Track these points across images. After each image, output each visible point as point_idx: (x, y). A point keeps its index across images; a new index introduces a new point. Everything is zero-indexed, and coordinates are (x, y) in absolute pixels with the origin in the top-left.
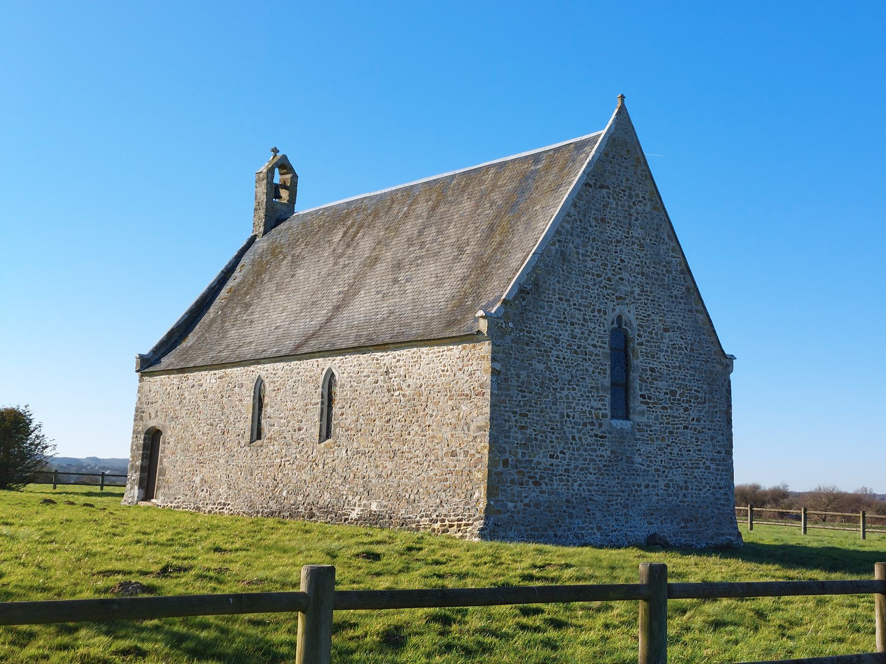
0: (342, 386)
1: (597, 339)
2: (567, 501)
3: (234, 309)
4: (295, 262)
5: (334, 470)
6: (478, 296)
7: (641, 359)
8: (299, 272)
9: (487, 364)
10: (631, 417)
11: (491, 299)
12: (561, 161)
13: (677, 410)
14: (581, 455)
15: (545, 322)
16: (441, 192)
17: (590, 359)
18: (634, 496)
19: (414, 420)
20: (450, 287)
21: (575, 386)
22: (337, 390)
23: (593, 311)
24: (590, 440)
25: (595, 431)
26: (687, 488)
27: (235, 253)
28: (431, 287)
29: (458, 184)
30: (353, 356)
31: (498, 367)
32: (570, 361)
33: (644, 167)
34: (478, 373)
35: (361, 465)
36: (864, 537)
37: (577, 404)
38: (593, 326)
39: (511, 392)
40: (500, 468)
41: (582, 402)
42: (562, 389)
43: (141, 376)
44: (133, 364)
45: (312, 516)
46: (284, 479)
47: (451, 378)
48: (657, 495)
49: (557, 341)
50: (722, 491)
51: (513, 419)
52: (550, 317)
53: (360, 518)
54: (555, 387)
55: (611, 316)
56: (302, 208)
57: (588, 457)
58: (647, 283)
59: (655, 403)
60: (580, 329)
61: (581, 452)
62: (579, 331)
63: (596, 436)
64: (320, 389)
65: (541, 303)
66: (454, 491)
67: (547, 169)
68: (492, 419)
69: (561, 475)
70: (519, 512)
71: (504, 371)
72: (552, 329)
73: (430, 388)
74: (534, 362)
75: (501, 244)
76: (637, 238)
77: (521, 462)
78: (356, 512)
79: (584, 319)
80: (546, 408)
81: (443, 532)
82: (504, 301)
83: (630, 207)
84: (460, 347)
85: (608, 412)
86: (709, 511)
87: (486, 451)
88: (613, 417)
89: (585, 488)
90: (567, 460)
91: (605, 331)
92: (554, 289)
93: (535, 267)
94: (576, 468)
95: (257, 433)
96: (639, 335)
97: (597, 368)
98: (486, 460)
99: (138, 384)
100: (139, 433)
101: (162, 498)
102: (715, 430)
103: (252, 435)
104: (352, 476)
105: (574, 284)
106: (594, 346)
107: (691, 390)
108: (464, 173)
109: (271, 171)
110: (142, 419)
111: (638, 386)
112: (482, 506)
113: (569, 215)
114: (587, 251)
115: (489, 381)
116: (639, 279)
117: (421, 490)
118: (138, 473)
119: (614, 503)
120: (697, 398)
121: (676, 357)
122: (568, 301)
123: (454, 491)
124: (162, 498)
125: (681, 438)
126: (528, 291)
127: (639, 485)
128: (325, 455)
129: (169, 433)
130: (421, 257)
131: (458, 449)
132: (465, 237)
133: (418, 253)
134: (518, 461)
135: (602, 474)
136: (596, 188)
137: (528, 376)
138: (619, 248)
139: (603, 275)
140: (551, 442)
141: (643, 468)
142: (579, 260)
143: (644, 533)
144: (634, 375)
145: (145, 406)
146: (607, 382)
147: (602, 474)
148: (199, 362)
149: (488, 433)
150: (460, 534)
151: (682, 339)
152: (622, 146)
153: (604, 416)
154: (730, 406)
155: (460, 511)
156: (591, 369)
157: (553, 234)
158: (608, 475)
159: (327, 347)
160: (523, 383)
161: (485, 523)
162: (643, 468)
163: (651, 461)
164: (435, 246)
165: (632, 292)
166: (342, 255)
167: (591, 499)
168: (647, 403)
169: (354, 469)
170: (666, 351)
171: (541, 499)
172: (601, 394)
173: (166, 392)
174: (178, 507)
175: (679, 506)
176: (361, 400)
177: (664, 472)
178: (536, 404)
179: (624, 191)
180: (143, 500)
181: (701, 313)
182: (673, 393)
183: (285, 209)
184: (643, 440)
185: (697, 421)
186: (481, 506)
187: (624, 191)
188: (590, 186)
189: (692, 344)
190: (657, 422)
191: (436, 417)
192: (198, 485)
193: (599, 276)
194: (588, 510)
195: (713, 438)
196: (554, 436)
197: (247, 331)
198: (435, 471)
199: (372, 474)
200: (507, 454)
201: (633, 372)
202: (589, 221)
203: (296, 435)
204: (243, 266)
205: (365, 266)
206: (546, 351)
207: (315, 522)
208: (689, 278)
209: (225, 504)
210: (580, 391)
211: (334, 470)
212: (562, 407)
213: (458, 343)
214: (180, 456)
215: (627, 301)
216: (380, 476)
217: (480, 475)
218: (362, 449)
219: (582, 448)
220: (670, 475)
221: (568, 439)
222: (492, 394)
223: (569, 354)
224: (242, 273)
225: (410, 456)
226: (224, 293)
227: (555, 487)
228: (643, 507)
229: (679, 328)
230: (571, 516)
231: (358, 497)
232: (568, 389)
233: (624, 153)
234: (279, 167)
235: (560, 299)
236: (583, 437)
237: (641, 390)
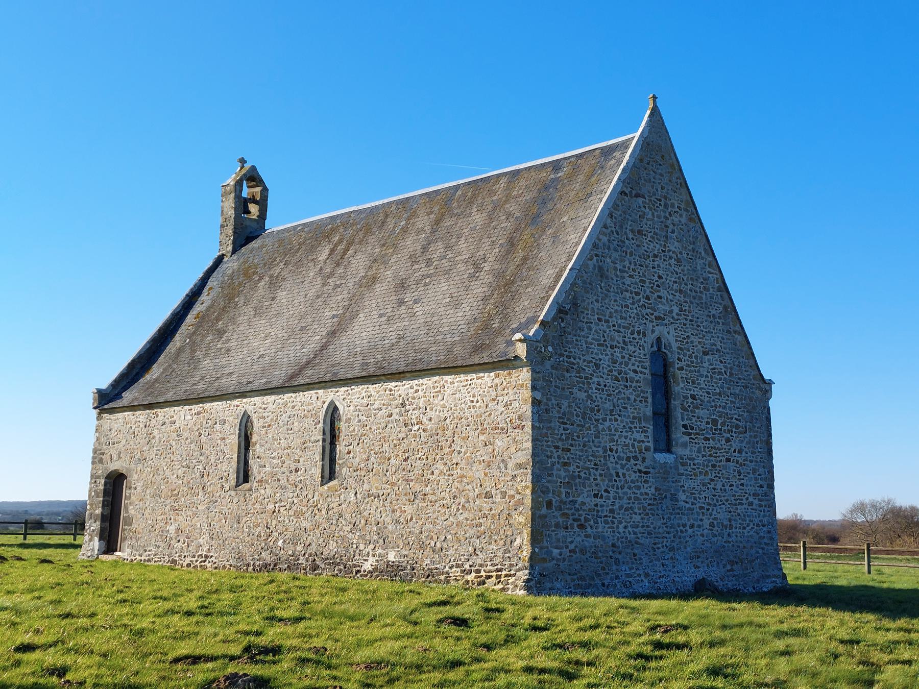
0: (348, 421)
1: (637, 364)
2: (613, 545)
3: (205, 336)
4: (275, 283)
5: (341, 516)
6: (505, 318)
7: (682, 385)
8: (280, 294)
9: (527, 394)
10: (673, 449)
11: (523, 320)
12: (587, 169)
13: (719, 441)
14: (625, 493)
15: (584, 346)
16: (445, 204)
17: (631, 386)
18: (680, 538)
19: (437, 458)
20: (469, 307)
21: (617, 416)
22: (342, 425)
23: (632, 333)
24: (634, 476)
25: (638, 467)
26: (731, 527)
27: (201, 275)
28: (447, 307)
29: (464, 195)
30: (361, 387)
31: (539, 396)
32: (611, 389)
33: (679, 174)
34: (515, 404)
35: (373, 509)
36: (869, 572)
37: (620, 436)
38: (633, 349)
39: (552, 425)
40: (544, 511)
41: (624, 434)
42: (604, 420)
43: (100, 414)
44: (89, 400)
45: (315, 568)
46: (280, 527)
47: (482, 410)
48: (702, 535)
49: (597, 366)
50: (765, 529)
51: (556, 455)
52: (589, 340)
53: (375, 570)
54: (596, 417)
55: (651, 338)
56: (273, 225)
57: (633, 496)
58: (686, 302)
59: (697, 434)
60: (620, 352)
61: (626, 490)
62: (620, 355)
63: (640, 471)
64: (321, 425)
65: (580, 324)
66: (490, 537)
67: (570, 177)
68: (534, 455)
69: (606, 516)
70: (564, 560)
71: (545, 401)
72: (592, 353)
73: (456, 421)
74: (575, 390)
75: (525, 259)
76: (674, 252)
77: (565, 503)
78: (370, 563)
79: (624, 342)
80: (589, 441)
81: (479, 584)
82: (543, 323)
83: (667, 218)
84: (492, 374)
85: (651, 444)
86: (753, 551)
87: (528, 492)
88: (656, 450)
89: (630, 529)
90: (612, 500)
91: (645, 355)
92: (593, 308)
93: (574, 284)
94: (621, 507)
95: (244, 475)
96: (679, 359)
97: (638, 396)
98: (528, 501)
99: (96, 422)
100: (98, 477)
101: (128, 551)
102: (756, 462)
103: (238, 478)
104: (363, 522)
105: (612, 302)
106: (635, 371)
107: (732, 418)
108: (469, 183)
109: (239, 184)
110: (101, 461)
111: (679, 415)
112: (526, 553)
113: (605, 227)
114: (624, 267)
115: (529, 413)
116: (677, 297)
117: (449, 537)
118: (98, 523)
119: (660, 546)
120: (737, 427)
121: (716, 383)
122: (607, 321)
123: (490, 537)
124: (128, 551)
125: (724, 472)
126: (567, 311)
127: (684, 526)
128: (329, 499)
129: (136, 477)
130: (429, 276)
131: (493, 490)
132: (481, 253)
133: (424, 271)
134: (561, 501)
135: (647, 514)
136: (632, 197)
137: (569, 406)
138: (656, 263)
139: (642, 293)
140: (595, 479)
141: (688, 506)
142: (617, 276)
143: (691, 579)
144: (675, 403)
145: (105, 447)
146: (649, 411)
147: (647, 514)
148: (170, 396)
149: (530, 471)
150: (500, 586)
151: (721, 362)
152: (657, 150)
153: (647, 449)
154: (770, 435)
155: (498, 560)
156: (632, 397)
157: (590, 247)
158: (653, 515)
159: (328, 377)
160: (564, 414)
161: (530, 574)
162: (688, 506)
163: (695, 499)
164: (445, 264)
165: (671, 312)
166: (332, 274)
167: (637, 543)
168: (690, 434)
169: (366, 514)
170: (706, 376)
171: (587, 544)
172: (643, 424)
173: (131, 431)
174: (149, 560)
175: (724, 547)
176: (371, 435)
177: (708, 510)
178: (578, 437)
179: (660, 200)
180: (104, 553)
181: (739, 334)
182: (715, 422)
183: (254, 225)
184: (687, 475)
185: (739, 452)
186: (525, 553)
187: (660, 200)
188: (626, 194)
189: (731, 368)
190: (700, 455)
191: (465, 453)
192: (173, 535)
193: (637, 294)
194: (635, 555)
195: (754, 471)
196: (597, 473)
197: (224, 361)
198: (466, 515)
199: (388, 520)
200: (551, 495)
201: (674, 400)
202: (626, 233)
203: (292, 477)
204: (211, 288)
205: (361, 286)
206: (586, 378)
207: (320, 574)
208: (725, 294)
209: (206, 557)
210: (622, 421)
211: (341, 516)
212: (605, 440)
213: (489, 371)
214: (149, 501)
215: (666, 321)
216: (398, 521)
217: (522, 518)
218: (374, 491)
219: (626, 486)
220: (714, 512)
221: (611, 475)
222: (533, 427)
223: (610, 381)
224: (210, 297)
225: (434, 498)
226: (190, 319)
227: (600, 530)
228: (689, 549)
229: (718, 350)
230: (617, 562)
231: (372, 546)
232: (611, 420)
233: (658, 158)
234: (247, 180)
235: (599, 320)
236: (627, 473)
237: (683, 420)
